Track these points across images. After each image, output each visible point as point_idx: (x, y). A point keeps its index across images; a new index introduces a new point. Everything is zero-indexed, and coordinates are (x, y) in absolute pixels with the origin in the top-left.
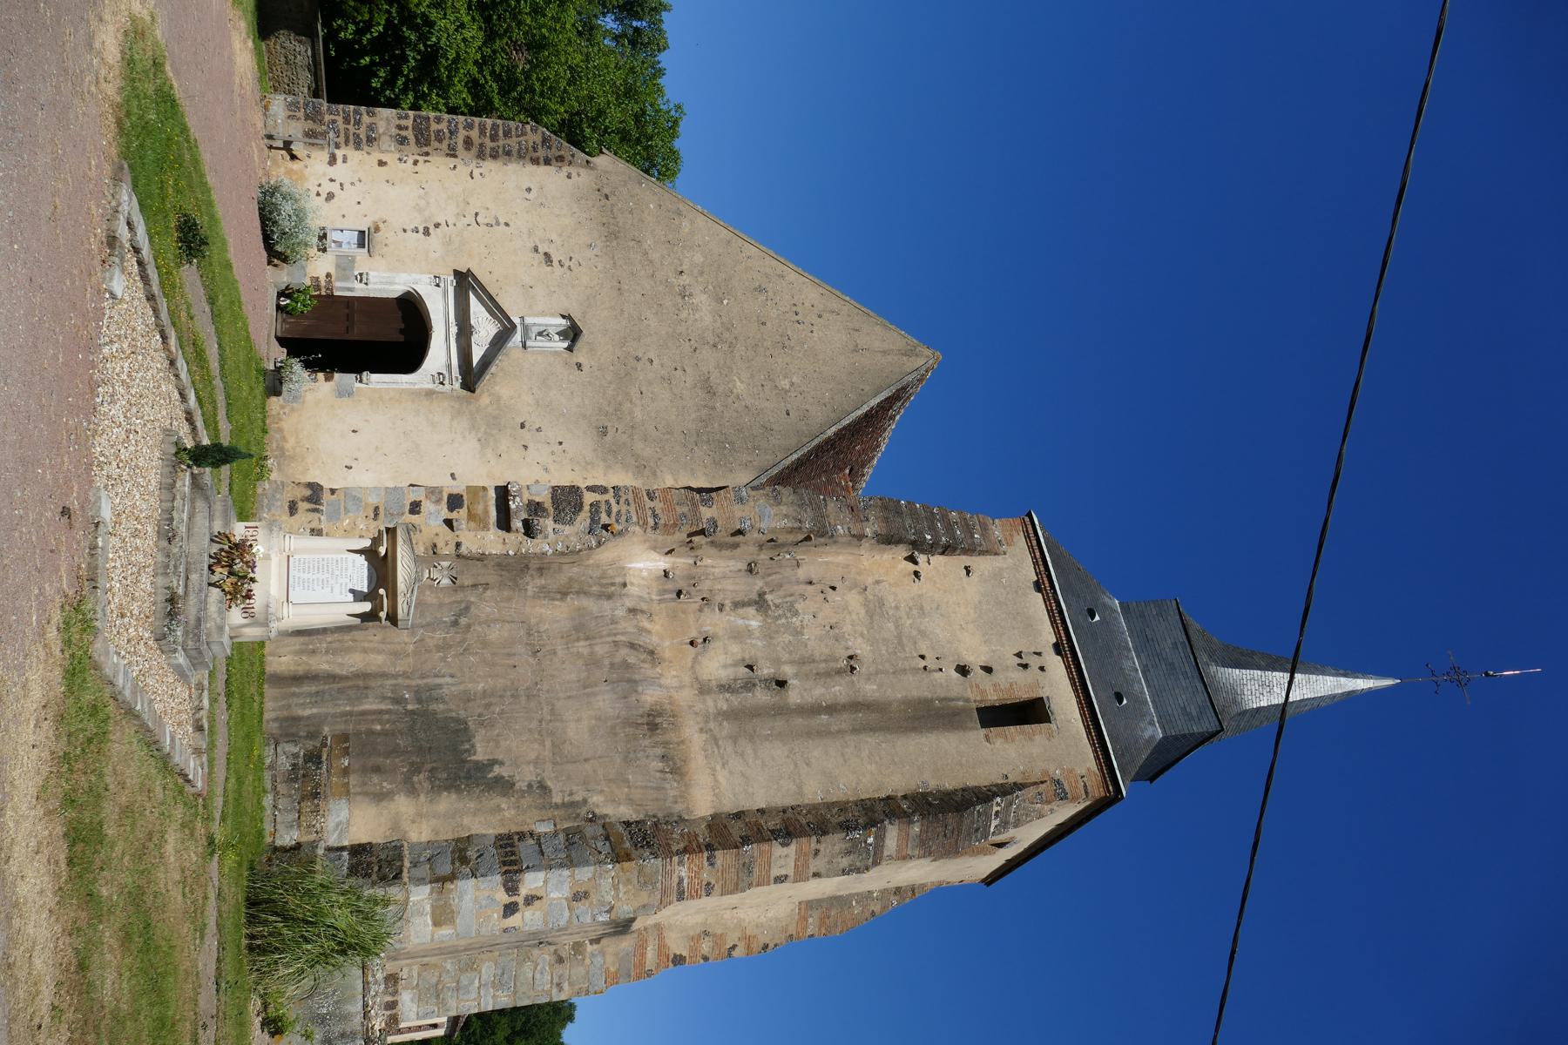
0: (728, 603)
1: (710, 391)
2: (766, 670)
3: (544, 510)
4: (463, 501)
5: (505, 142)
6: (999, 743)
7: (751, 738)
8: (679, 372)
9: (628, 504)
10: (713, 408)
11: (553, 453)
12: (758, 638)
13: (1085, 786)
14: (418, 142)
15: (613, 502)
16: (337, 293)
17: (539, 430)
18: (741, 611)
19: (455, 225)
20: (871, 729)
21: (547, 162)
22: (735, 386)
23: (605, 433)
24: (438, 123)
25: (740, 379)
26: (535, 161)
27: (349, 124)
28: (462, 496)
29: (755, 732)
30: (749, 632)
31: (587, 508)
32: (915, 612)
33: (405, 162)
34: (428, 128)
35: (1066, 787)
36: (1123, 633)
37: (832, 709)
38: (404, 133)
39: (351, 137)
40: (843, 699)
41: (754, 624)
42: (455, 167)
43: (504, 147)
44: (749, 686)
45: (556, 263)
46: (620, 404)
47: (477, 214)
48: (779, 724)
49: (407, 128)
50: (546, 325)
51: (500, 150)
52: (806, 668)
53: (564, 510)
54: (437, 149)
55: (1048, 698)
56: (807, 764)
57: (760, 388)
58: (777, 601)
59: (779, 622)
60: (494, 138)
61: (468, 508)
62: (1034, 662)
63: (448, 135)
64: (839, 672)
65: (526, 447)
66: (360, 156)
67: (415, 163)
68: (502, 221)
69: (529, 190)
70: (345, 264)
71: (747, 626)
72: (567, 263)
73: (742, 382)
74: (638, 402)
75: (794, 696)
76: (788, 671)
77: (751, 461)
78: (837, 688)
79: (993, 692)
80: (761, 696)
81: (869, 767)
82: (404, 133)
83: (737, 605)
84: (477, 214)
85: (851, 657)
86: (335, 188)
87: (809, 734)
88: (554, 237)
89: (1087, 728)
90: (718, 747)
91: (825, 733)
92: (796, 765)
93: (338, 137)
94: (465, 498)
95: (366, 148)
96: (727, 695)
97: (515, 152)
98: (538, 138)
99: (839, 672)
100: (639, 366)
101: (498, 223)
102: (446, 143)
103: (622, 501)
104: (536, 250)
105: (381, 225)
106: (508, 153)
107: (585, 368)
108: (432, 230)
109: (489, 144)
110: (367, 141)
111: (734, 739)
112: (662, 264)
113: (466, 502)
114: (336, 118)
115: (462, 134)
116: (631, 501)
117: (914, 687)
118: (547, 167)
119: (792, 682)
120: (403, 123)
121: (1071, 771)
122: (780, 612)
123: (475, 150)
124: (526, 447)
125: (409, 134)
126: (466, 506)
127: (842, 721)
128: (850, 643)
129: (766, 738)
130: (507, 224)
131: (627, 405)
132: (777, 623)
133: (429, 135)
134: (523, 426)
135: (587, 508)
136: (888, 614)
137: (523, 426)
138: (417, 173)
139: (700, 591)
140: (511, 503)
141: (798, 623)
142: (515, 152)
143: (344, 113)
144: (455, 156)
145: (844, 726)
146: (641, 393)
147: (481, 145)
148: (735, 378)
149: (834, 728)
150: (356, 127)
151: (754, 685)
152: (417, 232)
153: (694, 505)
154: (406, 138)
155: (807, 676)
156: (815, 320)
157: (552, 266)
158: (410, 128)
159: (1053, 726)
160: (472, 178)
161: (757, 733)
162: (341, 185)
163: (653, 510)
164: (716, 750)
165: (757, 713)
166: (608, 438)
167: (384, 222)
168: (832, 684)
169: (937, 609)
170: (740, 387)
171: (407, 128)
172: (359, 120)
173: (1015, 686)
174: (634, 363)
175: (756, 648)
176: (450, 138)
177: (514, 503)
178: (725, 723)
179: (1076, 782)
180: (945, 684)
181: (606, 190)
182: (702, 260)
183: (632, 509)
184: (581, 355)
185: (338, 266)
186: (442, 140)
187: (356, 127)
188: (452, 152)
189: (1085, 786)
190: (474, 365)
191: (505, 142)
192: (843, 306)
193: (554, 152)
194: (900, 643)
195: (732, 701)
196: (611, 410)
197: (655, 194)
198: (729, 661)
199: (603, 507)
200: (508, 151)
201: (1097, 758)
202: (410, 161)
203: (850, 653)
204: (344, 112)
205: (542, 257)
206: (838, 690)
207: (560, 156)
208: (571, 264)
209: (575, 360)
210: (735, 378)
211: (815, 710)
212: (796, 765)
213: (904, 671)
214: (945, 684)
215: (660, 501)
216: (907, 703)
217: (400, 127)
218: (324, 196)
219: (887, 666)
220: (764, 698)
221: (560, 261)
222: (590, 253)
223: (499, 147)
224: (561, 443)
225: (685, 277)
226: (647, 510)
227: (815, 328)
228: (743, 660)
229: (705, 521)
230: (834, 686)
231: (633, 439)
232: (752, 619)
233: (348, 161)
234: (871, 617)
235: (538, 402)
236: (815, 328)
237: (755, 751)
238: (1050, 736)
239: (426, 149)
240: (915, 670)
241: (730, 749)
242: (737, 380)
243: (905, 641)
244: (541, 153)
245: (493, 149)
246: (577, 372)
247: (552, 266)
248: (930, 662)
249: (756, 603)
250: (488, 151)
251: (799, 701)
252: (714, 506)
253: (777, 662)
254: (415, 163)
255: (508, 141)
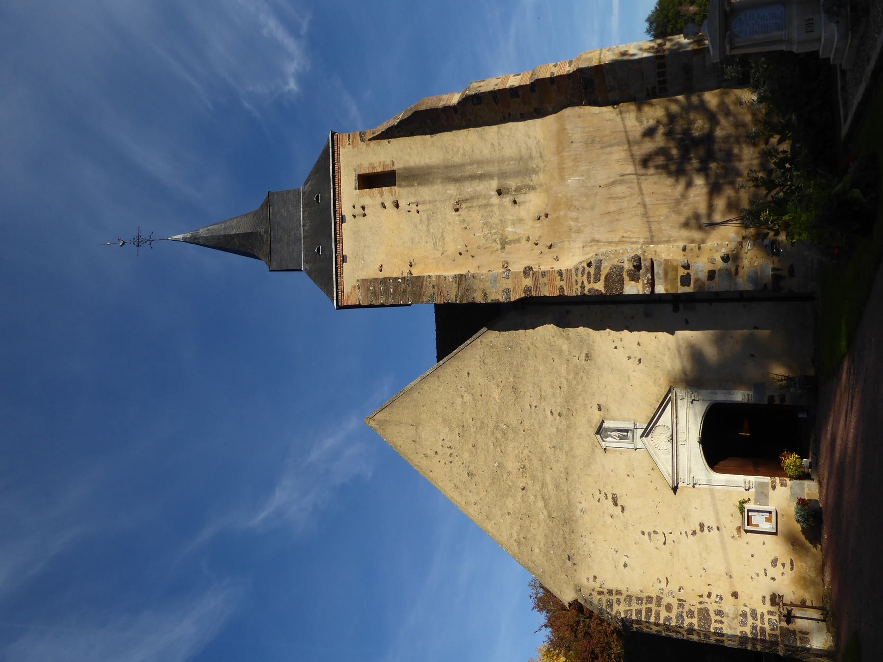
0: (523, 241)
1: (515, 389)
2: (507, 200)
3: (629, 275)
4: (681, 281)
5: (641, 607)
6: (388, 162)
7: (521, 158)
8: (534, 404)
9: (576, 281)
10: (514, 377)
11: (621, 340)
12: (509, 220)
13: (349, 139)
14: (707, 611)
15: (586, 283)
16: (769, 478)
17: (629, 358)
18: (516, 237)
19: (681, 534)
20: (455, 166)
21: (610, 592)
22: (499, 394)
23: (587, 355)
24: (691, 623)
25: (495, 400)
26: (619, 592)
27: (761, 627)
28: (681, 285)
29: (519, 162)
30: (513, 223)
31: (603, 278)
32: (417, 240)
33: (717, 596)
34: (700, 620)
35: (359, 137)
36: (304, 248)
37: (473, 177)
38: (718, 618)
39: (759, 618)
40: (467, 184)
41: (510, 229)
42: (680, 590)
43: (642, 603)
44: (518, 190)
45: (610, 497)
46: (575, 378)
47: (665, 543)
48: (505, 167)
49: (716, 621)
50: (620, 442)
51: (645, 601)
52: (484, 202)
53: (617, 276)
54: (693, 605)
55: (356, 189)
56: (493, 144)
57: (483, 393)
58: (494, 244)
59: (495, 231)
60: (649, 610)
61: (677, 276)
62: (359, 210)
63: (684, 615)
64: (466, 200)
65: (639, 344)
66: (752, 603)
67: (709, 595)
68: (646, 536)
69: (625, 566)
70: (762, 495)
71: (514, 228)
72: (602, 496)
73: (494, 398)
74: (563, 380)
75: (494, 184)
76: (495, 200)
77: (497, 337)
78: (469, 190)
79: (385, 194)
80: (512, 183)
81: (460, 145)
82: (718, 618)
83: (518, 241)
84: (665, 543)
85: (457, 210)
86: (771, 572)
87: (488, 162)
88: (609, 520)
89: (339, 172)
90: (541, 152)
91: (480, 163)
92: (499, 144)
93: (769, 619)
94: (679, 284)
95: (748, 610)
96: (531, 184)
97: (634, 600)
98: (616, 607)
99: (466, 200)
100: (559, 410)
101: (649, 534)
102: (686, 609)
103: (580, 284)
104: (623, 508)
105: (735, 533)
106: (639, 599)
107: (596, 407)
108: (698, 528)
109: (653, 606)
110: (746, 614)
111: (531, 157)
112: (536, 496)
113: (679, 280)
114: (771, 632)
115: (673, 615)
116: (574, 283)
117: (425, 192)
118: (610, 588)
119: (494, 193)
120: (718, 625)
121: (354, 147)
122: (494, 237)
123: (664, 602)
124: (639, 344)
125: (714, 617)
126: (679, 278)
127: (469, 170)
128: (457, 218)
129: (513, 159)
130: (643, 533)
131: (570, 377)
132: (497, 230)
133: (698, 615)
134: (640, 361)
135: (603, 278)
136: (433, 238)
137: (640, 361)
138: (709, 585)
139: (539, 249)
140: (650, 277)
141: (485, 230)
142: (634, 600)
143: (765, 635)
144: (679, 600)
145: (469, 168)
146: (560, 387)
147: (659, 606)
148: (498, 401)
149: (475, 166)
150: (755, 625)
151: (515, 191)
152: (709, 527)
153: (536, 286)
154: (717, 615)
155: (485, 197)
156: (439, 450)
157: (613, 494)
158: (713, 621)
159: (357, 173)
160: (667, 578)
161: (518, 161)
162: (766, 575)
163: (562, 280)
164: (542, 151)
165: (517, 174)
166: (585, 351)
167: (733, 537)
168: (471, 193)
169: (404, 242)
170: (496, 394)
171: (716, 621)
172: (753, 630)
173: (372, 195)
174: (564, 412)
175: (513, 213)
176: (682, 612)
177: (648, 278)
178: (535, 167)
179: (353, 141)
180: (410, 195)
181: (569, 563)
182: (508, 501)
183: (574, 278)
184: (596, 417)
185: (767, 496)
186: (688, 611)
187: (755, 625)
188: (681, 602)
189: (349, 139)
190: (677, 97)
191: (641, 607)
192: (419, 461)
193: (604, 598)
194: (429, 219)
195: (529, 180)
196: (582, 373)
197: (533, 562)
198: (527, 204)
199: (592, 279)
200: (639, 600)
201: (338, 155)
202: (713, 596)
203: (457, 213)
204: (765, 636)
205: (619, 503)
206: (469, 188)
207: (600, 594)
208: (599, 496)
209: (601, 413)
210: (498, 401)
211: (481, 177)
212: (499, 144)
213: (430, 202)
214: (410, 195)
215: (556, 286)
216: (432, 183)
217: (721, 622)
218: (779, 564)
219: (439, 206)
220: (511, 183)
221: (607, 498)
222: (584, 505)
223: (646, 604)
224: (616, 348)
225: (521, 485)
226: (565, 279)
227: (441, 443)
228: (519, 206)
229: (531, 276)
230: (471, 191)
231: (569, 351)
232: (511, 232)
233: (761, 598)
234: (442, 236)
235: (629, 379)
236: (441, 443)
237: (520, 151)
238: (360, 166)
239: (702, 606)
240: (424, 203)
241: (534, 151)
242: (497, 400)
243: (426, 222)
244: (614, 598)
245: (651, 603)
246: (601, 403)
247: (613, 494)
248: (414, 208)
249: (507, 243)
250: (654, 602)
251: (492, 182)
252: (524, 286)
253: (501, 206)
254: (709, 595)
255: (639, 607)
